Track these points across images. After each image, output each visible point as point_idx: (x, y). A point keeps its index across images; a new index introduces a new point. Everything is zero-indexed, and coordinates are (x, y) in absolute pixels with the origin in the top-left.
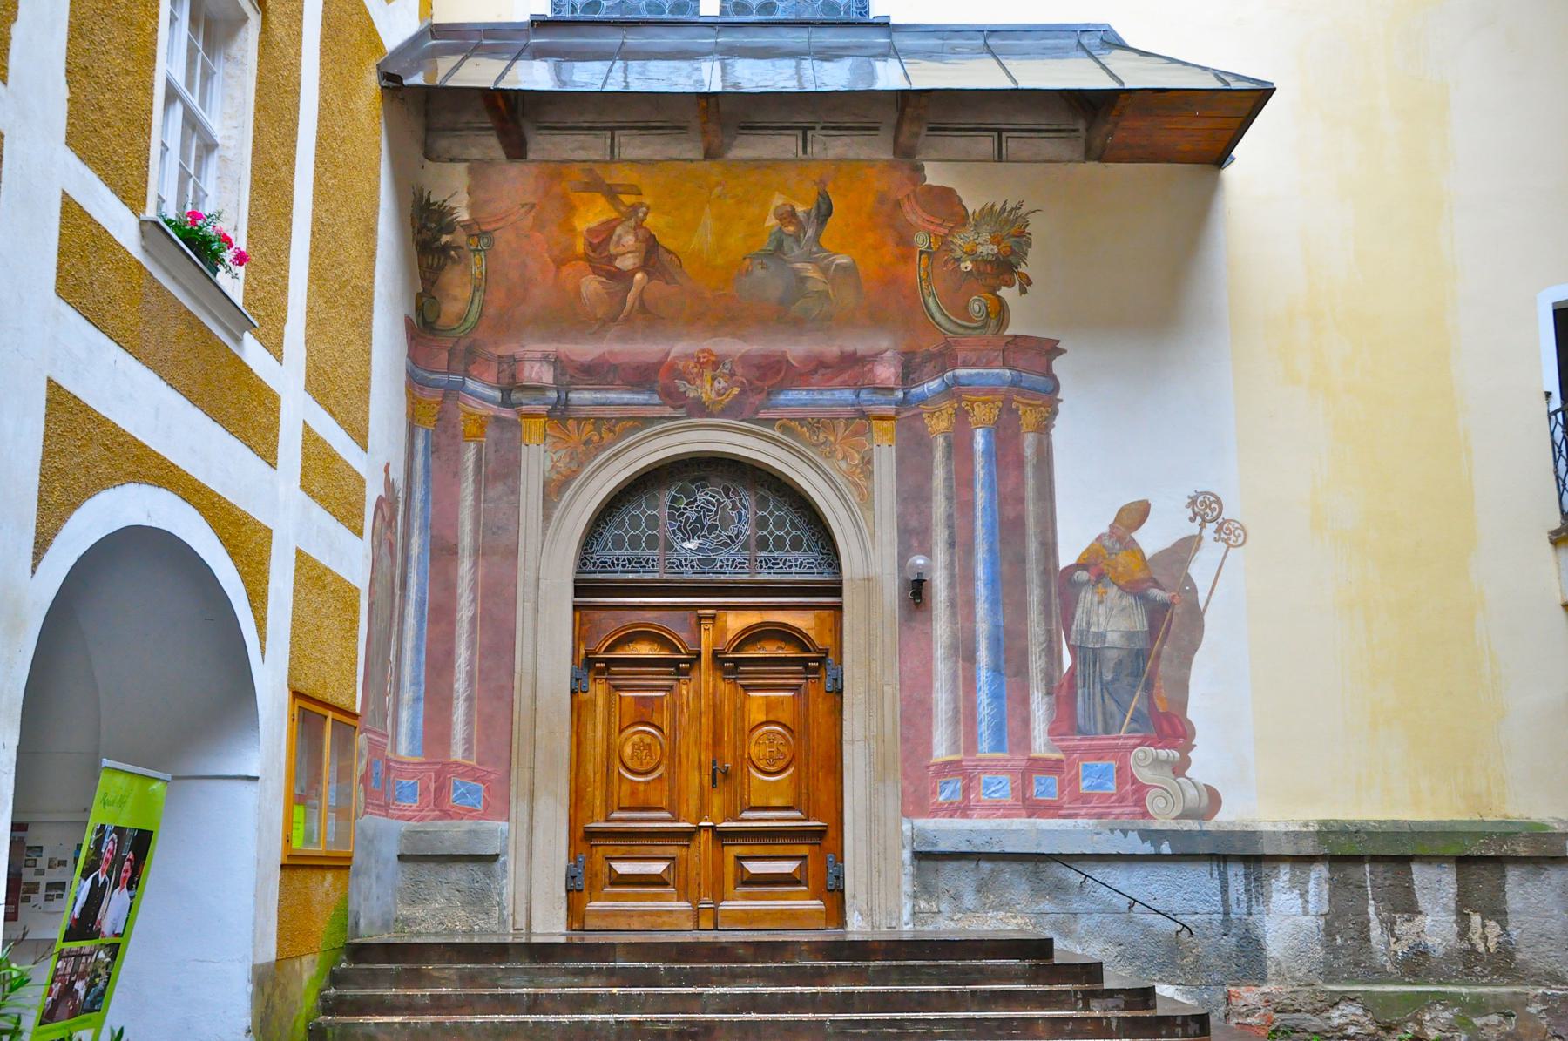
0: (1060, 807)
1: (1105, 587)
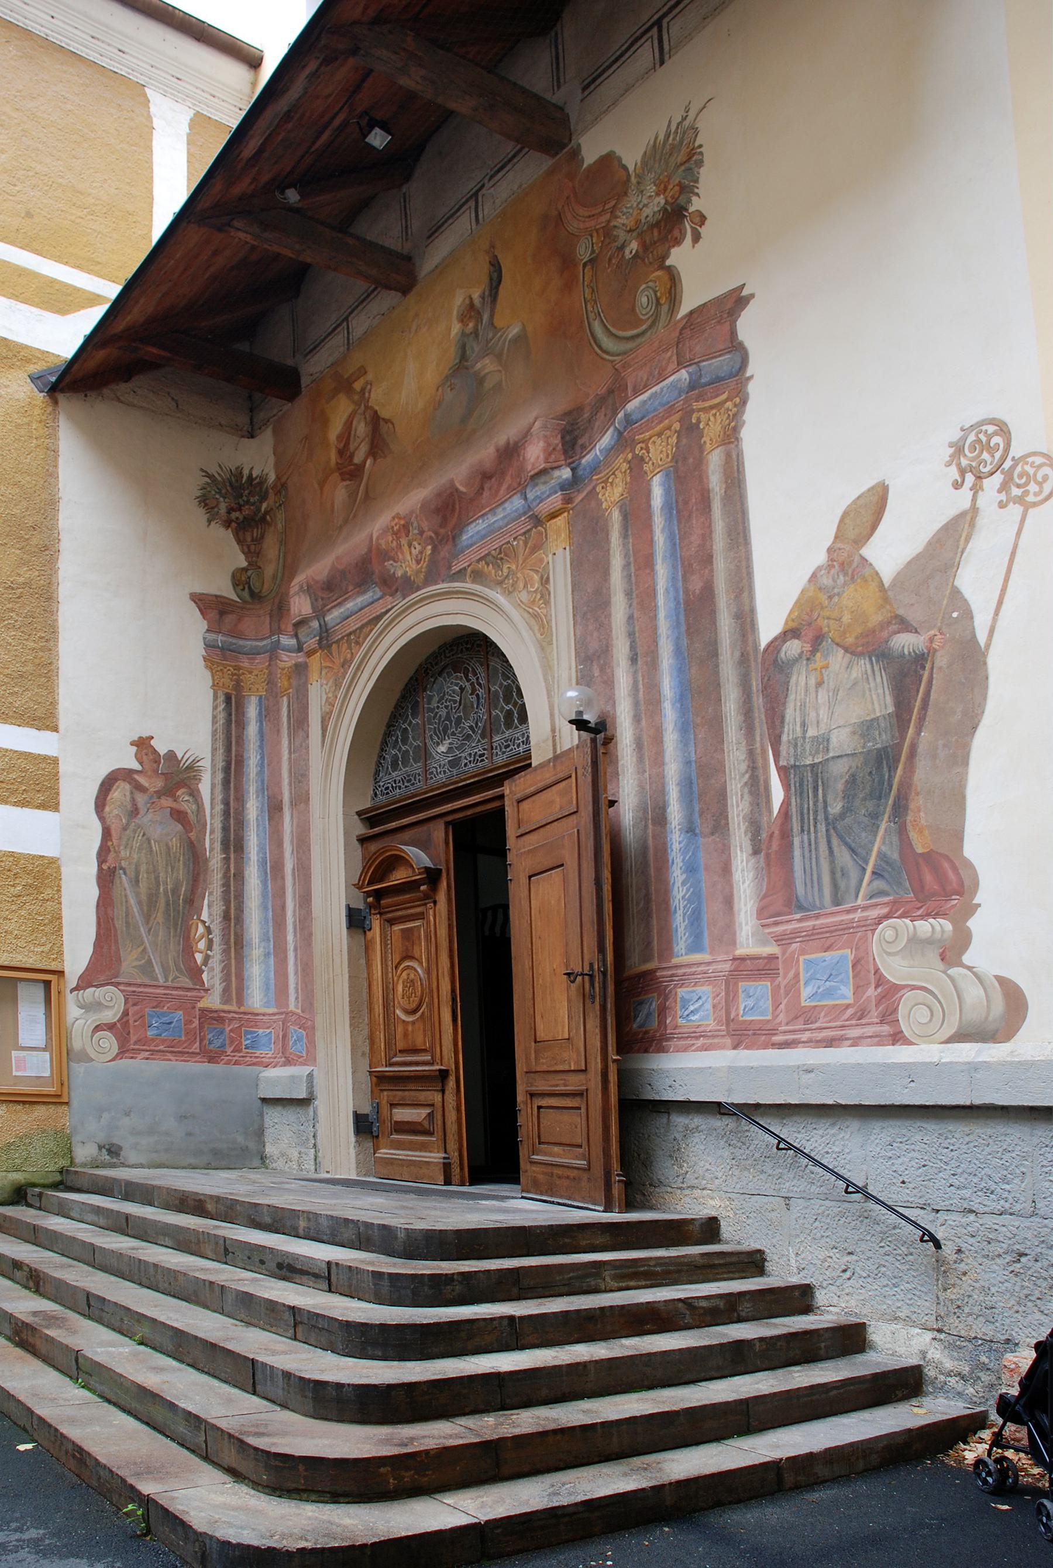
0: (773, 1032)
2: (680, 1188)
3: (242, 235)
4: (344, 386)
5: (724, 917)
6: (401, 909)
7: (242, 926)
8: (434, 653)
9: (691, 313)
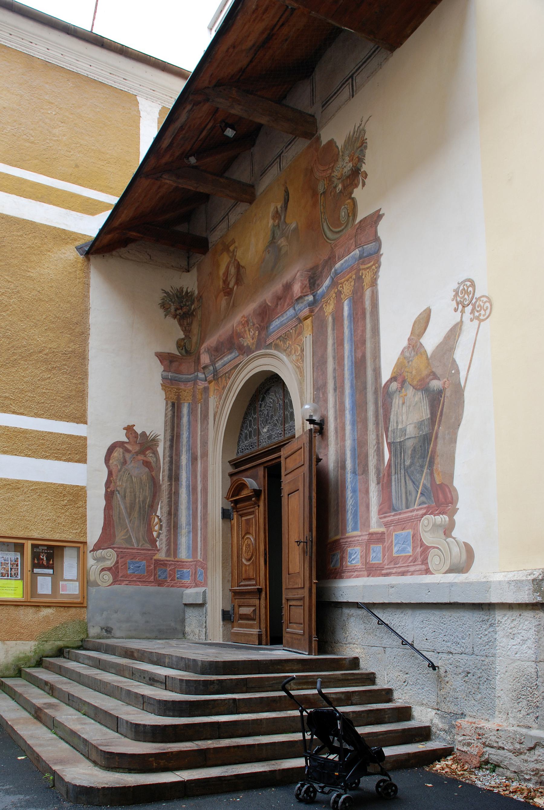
0: (382, 569)
1: (406, 390)
2: (345, 644)
3: (169, 182)
4: (226, 248)
5: (366, 514)
6: (245, 509)
7: (177, 518)
8: (263, 382)
9: (361, 221)
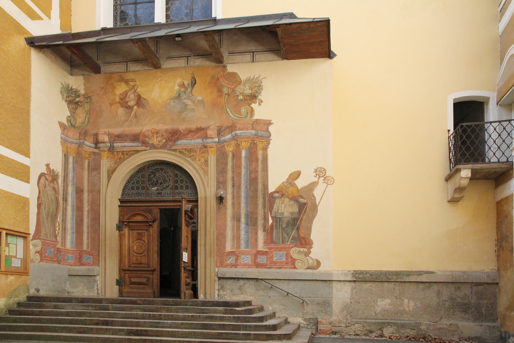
0: (266, 265)
